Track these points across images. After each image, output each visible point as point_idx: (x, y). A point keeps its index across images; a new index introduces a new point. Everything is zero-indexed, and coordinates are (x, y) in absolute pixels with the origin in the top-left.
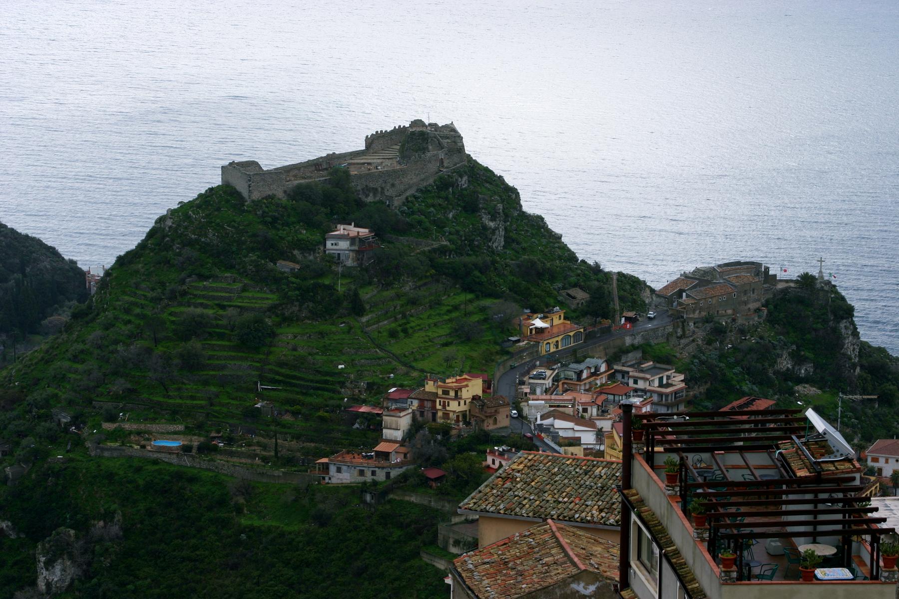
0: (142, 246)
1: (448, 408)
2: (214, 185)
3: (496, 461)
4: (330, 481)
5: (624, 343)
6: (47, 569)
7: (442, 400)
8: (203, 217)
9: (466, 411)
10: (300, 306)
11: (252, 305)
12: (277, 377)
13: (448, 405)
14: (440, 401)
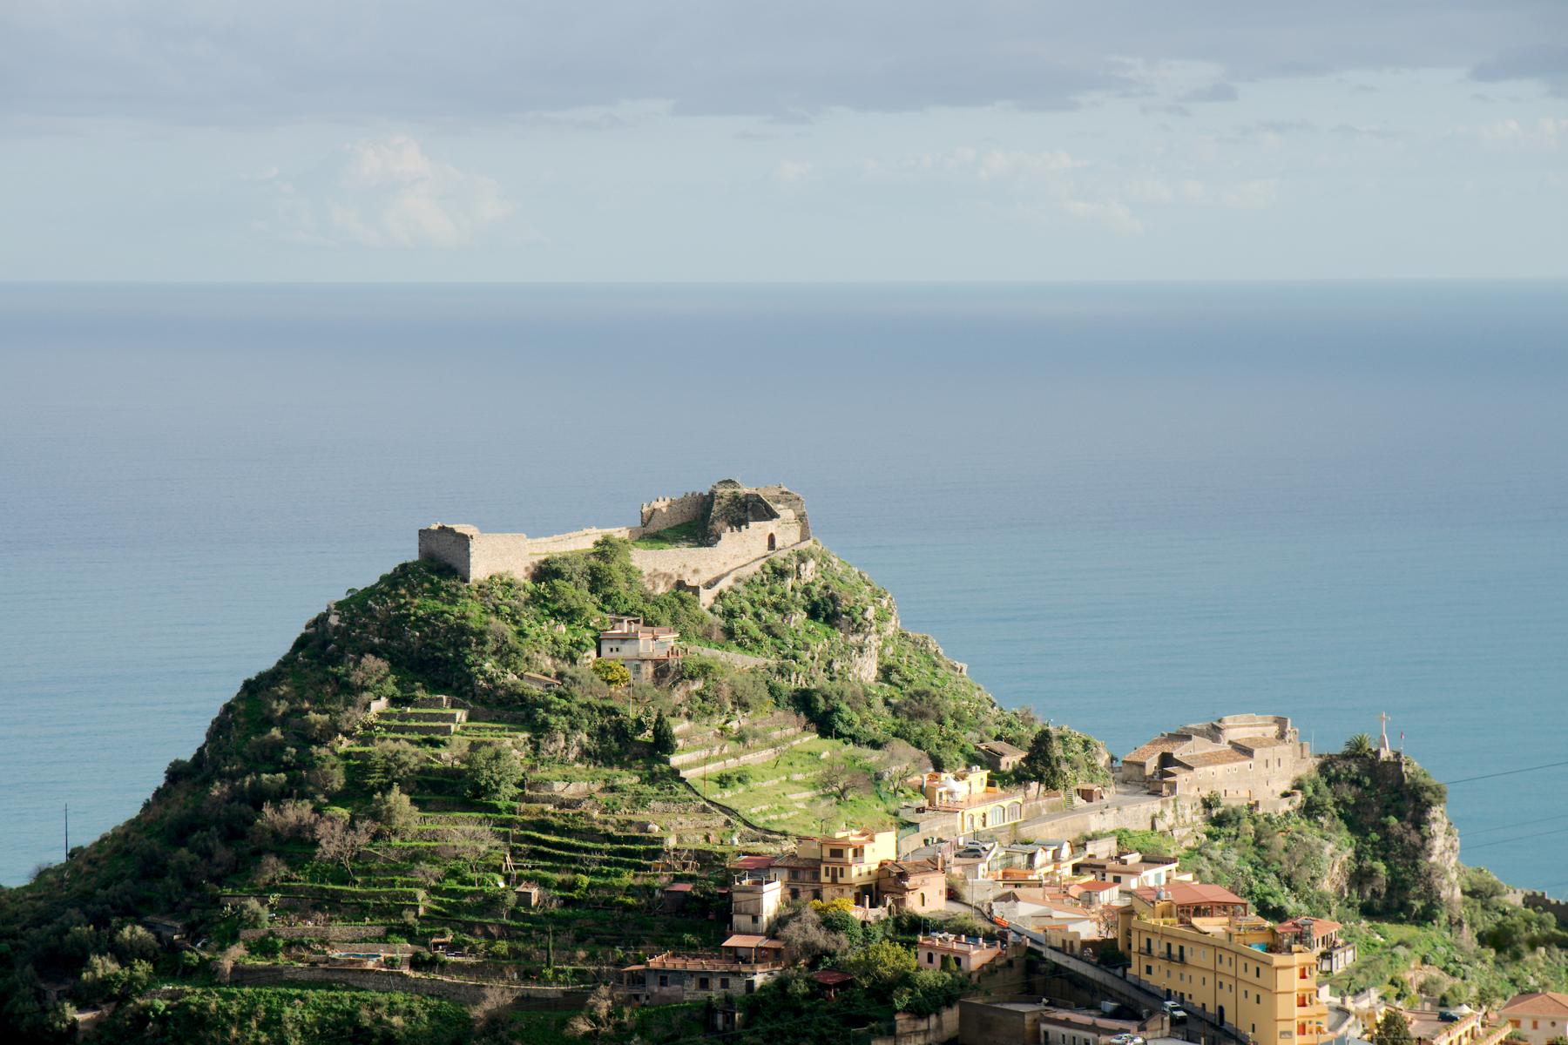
0: (287, 662)
1: (840, 880)
2: (410, 560)
3: (934, 956)
4: (648, 1002)
7: (830, 867)
9: (871, 885)
10: (566, 740)
11: (542, 863)
12: (541, 848)
13: (842, 875)
14: (827, 869)
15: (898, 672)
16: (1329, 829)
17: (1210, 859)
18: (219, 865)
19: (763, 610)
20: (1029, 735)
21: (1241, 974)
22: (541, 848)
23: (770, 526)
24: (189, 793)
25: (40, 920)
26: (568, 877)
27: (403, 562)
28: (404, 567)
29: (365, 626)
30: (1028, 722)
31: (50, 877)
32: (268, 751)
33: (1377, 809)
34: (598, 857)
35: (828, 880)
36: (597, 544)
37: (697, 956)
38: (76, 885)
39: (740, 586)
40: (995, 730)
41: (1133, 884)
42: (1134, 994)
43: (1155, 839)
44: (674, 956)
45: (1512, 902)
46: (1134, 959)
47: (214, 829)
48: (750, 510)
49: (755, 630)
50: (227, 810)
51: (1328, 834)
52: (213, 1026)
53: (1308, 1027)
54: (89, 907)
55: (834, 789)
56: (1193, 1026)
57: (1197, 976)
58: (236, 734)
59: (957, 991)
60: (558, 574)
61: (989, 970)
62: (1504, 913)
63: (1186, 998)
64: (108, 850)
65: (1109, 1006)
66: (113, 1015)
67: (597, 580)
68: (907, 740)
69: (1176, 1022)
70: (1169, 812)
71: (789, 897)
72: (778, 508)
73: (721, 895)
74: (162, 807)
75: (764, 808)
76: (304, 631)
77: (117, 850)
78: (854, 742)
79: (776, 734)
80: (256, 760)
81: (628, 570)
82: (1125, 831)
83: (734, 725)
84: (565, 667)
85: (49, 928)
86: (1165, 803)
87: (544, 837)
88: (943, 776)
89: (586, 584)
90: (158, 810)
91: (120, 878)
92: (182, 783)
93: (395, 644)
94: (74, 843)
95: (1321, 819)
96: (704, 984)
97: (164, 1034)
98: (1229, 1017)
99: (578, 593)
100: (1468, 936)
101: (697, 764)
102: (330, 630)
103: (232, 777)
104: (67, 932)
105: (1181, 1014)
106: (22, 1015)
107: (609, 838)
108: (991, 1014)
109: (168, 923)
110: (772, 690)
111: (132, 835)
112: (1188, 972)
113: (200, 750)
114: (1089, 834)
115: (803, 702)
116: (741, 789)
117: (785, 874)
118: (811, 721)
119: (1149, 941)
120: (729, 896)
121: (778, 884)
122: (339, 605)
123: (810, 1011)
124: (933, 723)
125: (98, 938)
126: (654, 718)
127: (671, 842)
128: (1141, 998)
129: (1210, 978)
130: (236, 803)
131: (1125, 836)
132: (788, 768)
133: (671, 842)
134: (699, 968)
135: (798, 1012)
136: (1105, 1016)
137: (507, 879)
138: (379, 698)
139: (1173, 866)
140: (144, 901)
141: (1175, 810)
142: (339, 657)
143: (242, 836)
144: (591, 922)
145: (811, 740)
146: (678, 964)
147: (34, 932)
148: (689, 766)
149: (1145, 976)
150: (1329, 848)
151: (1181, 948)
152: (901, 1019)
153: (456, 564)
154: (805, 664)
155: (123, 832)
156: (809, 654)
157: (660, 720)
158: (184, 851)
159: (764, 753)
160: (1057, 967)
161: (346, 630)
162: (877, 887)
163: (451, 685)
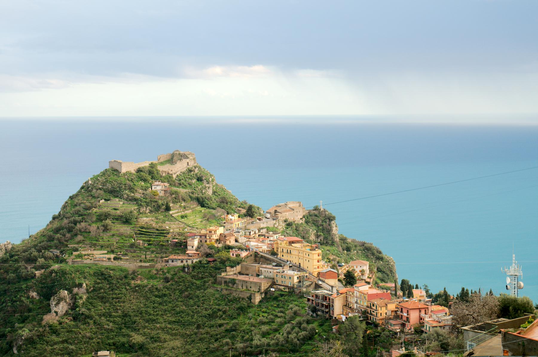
1: (211, 238)
5: (260, 226)
6: (56, 307)
8: (104, 179)
10: (146, 208)
12: (142, 232)
15: (217, 193)
16: (311, 226)
17: (287, 233)
18: (67, 238)
19: (187, 179)
20: (247, 206)
21: (305, 256)
22: (142, 232)
23: (188, 160)
24: (58, 222)
25: (25, 251)
26: (149, 239)
27: (106, 169)
28: (106, 170)
29: (98, 183)
30: (246, 203)
31: (26, 242)
32: (77, 212)
33: (321, 222)
34: (155, 234)
35: (209, 238)
36: (150, 164)
37: (180, 256)
38: (32, 243)
39: (181, 174)
40: (239, 205)
41: (272, 239)
42: (280, 261)
43: (275, 229)
44: (174, 256)
45: (349, 241)
46: (279, 254)
47: (65, 229)
48: (183, 157)
49: (185, 184)
50: (68, 226)
51: (310, 227)
52: (68, 274)
53: (320, 267)
54: (37, 248)
55: (208, 219)
56: (293, 267)
57: (294, 257)
58: (68, 208)
59: (240, 261)
60: (141, 171)
61: (247, 257)
62: (347, 244)
63: (292, 261)
64: (39, 235)
65: (274, 264)
66: (44, 272)
67: (150, 173)
68: (220, 207)
69: (290, 267)
70: (277, 223)
71: (200, 242)
72: (189, 156)
73: (184, 242)
74: (52, 225)
75: (192, 223)
76: (82, 185)
77: (42, 235)
78: (209, 208)
79: (192, 206)
80: (74, 214)
81: (157, 170)
82: (268, 227)
83: (182, 205)
84: (145, 192)
85: (27, 253)
86: (276, 221)
87: (142, 230)
88: (229, 215)
89: (148, 173)
90: (51, 226)
91: (43, 241)
92: (56, 220)
93: (105, 187)
94: (31, 234)
95: (309, 224)
96: (182, 262)
97: (57, 276)
98: (302, 265)
99: (146, 175)
100: (341, 249)
101: (176, 213)
102: (89, 185)
103: (69, 218)
104: (32, 254)
105: (291, 265)
106: (23, 272)
107: (157, 230)
108: (248, 266)
109: (56, 251)
110: (191, 197)
111: (45, 232)
112: (292, 256)
113: (60, 213)
114: (261, 228)
115: (198, 199)
116: (186, 219)
117: (199, 237)
118: (199, 203)
119: (283, 249)
120: (187, 242)
121: (197, 239)
122: (91, 179)
123: (207, 267)
124: (225, 204)
125: (39, 255)
126: (166, 203)
127: (172, 231)
128: (282, 262)
129: (297, 257)
130: (70, 224)
131: (268, 228)
132: (195, 214)
133: (172, 231)
134: (181, 258)
135: (204, 267)
136: (273, 266)
137: (134, 240)
138: (102, 200)
139: (280, 234)
140: (49, 246)
141: (278, 223)
142: (91, 191)
143: (72, 231)
144: (154, 249)
145: (199, 208)
146: (176, 257)
147: (24, 254)
148: (174, 214)
149: (282, 257)
150: (311, 230)
151: (290, 251)
152: (228, 268)
153: (118, 169)
154: (197, 191)
155: (43, 231)
156: (198, 189)
157: (167, 204)
158: (59, 235)
159: (189, 211)
160: (262, 256)
161: (93, 185)
162: (219, 240)
163: (118, 196)
